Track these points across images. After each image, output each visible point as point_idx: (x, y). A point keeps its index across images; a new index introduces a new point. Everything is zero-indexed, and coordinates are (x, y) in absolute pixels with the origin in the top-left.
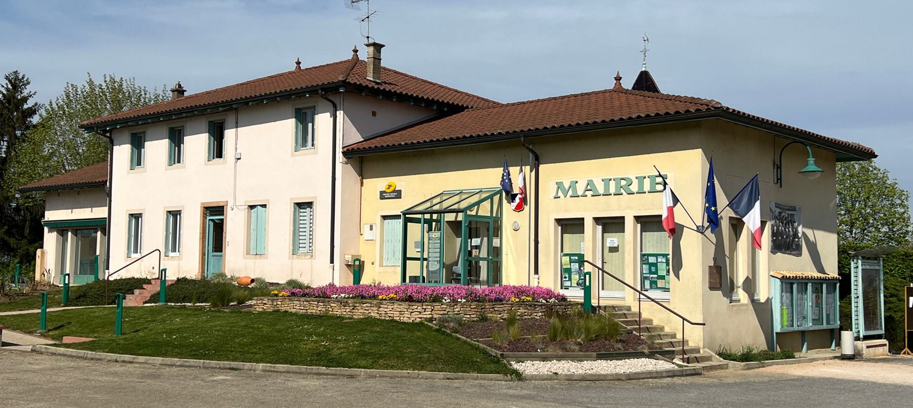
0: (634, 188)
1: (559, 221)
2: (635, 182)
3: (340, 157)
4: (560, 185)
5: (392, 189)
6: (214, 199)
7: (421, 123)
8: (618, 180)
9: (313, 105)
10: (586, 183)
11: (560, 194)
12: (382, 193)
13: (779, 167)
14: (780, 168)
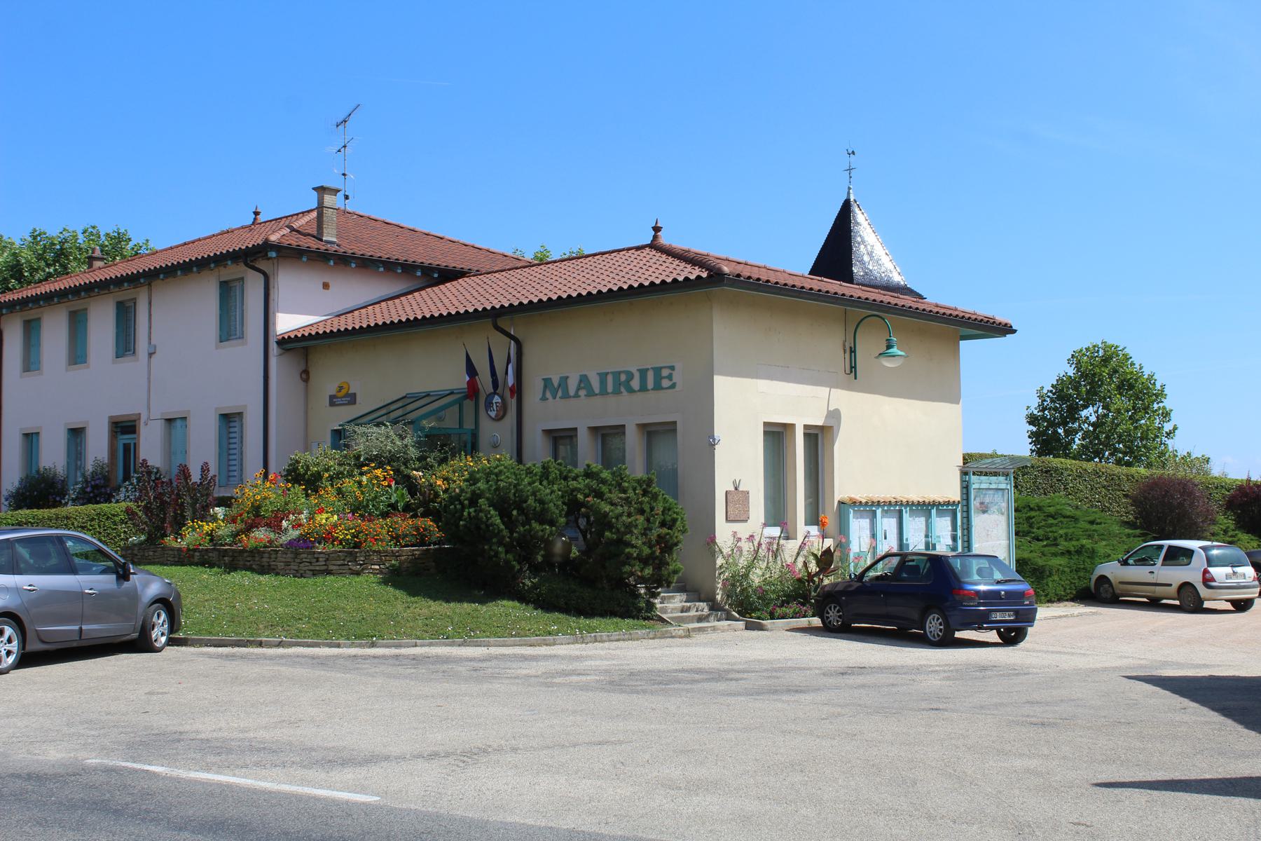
0: (635, 384)
2: (637, 376)
3: (274, 348)
4: (547, 382)
5: (344, 392)
6: (123, 409)
7: (150, 315)
8: (617, 375)
9: (239, 276)
11: (548, 395)
12: (332, 397)
13: (853, 351)
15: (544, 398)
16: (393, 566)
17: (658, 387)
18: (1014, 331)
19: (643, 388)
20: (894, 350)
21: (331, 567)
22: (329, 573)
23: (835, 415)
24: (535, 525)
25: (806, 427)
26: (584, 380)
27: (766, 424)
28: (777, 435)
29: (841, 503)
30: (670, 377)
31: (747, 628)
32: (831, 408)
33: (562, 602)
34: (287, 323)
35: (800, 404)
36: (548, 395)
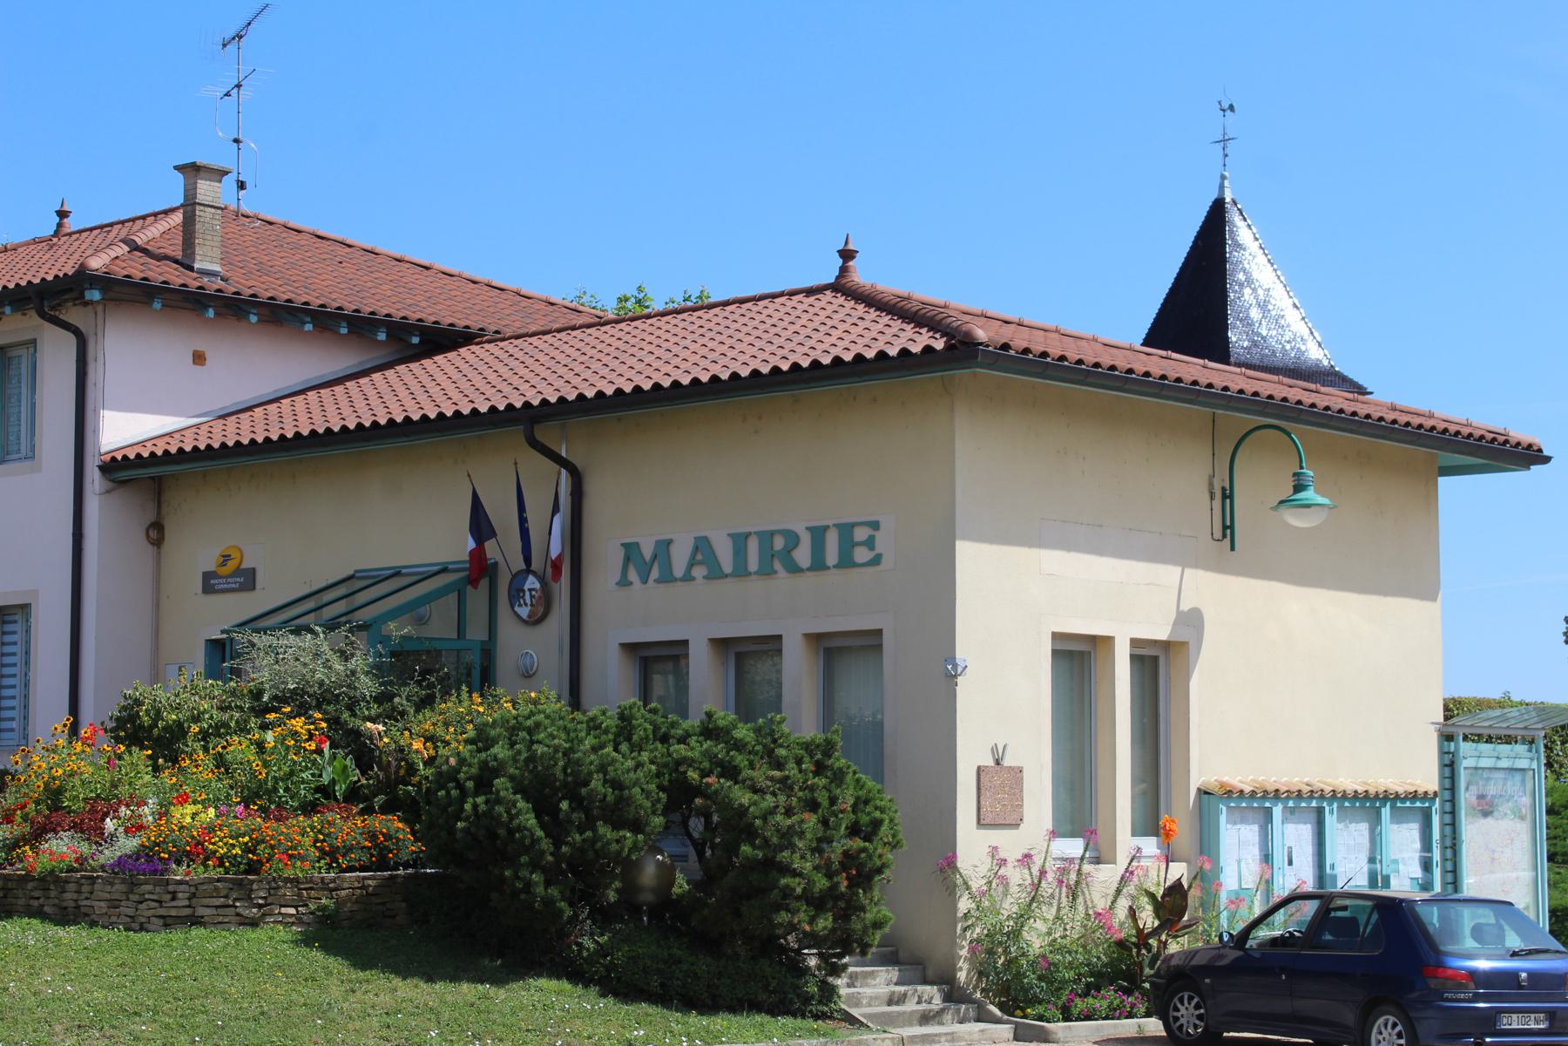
0: (803, 555)
1: (630, 648)
2: (806, 539)
4: (631, 551)
5: (232, 565)
8: (767, 537)
10: (691, 543)
11: (633, 575)
12: (207, 576)
13: (1228, 495)
14: (1231, 497)
15: (624, 582)
16: (324, 908)
17: (846, 562)
18: (1547, 460)
19: (818, 565)
20: (1309, 495)
21: (201, 911)
22: (196, 921)
23: (1191, 620)
24: (604, 830)
25: (1135, 643)
26: (703, 548)
27: (1056, 637)
28: (1077, 659)
29: (1203, 793)
30: (870, 543)
31: (1016, 1038)
32: (1185, 607)
33: (655, 982)
34: (120, 430)
35: (1125, 597)
36: (633, 575)
